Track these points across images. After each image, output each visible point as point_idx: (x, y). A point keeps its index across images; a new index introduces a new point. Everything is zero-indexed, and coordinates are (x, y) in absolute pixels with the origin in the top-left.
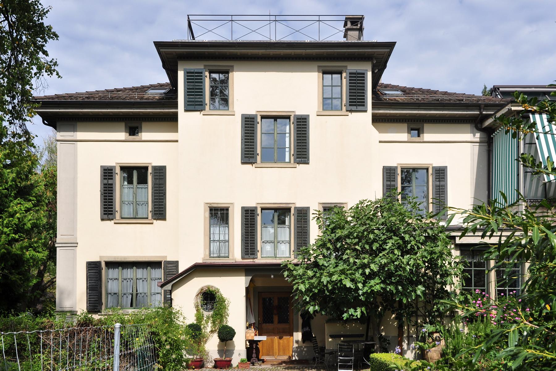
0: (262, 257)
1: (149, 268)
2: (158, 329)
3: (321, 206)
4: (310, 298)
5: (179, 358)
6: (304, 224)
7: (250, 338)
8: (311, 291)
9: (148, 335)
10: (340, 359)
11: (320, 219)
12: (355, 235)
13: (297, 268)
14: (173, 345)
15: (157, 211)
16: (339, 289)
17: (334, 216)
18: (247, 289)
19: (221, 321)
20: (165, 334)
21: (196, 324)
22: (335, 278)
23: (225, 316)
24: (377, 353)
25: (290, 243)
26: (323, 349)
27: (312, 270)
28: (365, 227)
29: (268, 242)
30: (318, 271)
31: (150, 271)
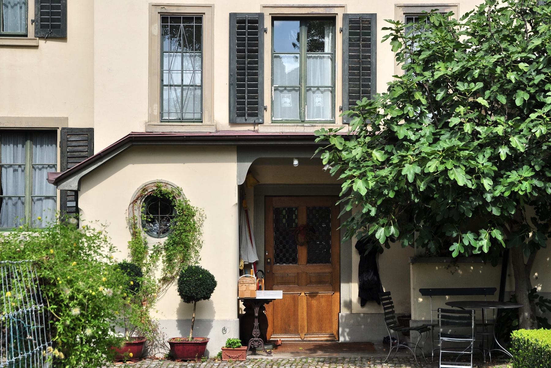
0: (273, 122)
1: (28, 143)
2: (55, 273)
3: (401, 12)
4: (379, 209)
5: (99, 335)
6: (364, 51)
7: (247, 295)
8: (381, 195)
9: (32, 286)
10: (444, 342)
11: (400, 40)
12: (476, 73)
13: (350, 144)
14: (88, 307)
15: (47, 20)
16: (442, 189)
17: (429, 34)
18: (242, 189)
19: (185, 258)
20: (70, 282)
21: (130, 264)
22: (432, 166)
23: (193, 247)
24: (526, 329)
25: (333, 92)
26: (405, 318)
27: (383, 149)
28: (497, 56)
29: (285, 89)
30: (394, 151)
31: (31, 149)
